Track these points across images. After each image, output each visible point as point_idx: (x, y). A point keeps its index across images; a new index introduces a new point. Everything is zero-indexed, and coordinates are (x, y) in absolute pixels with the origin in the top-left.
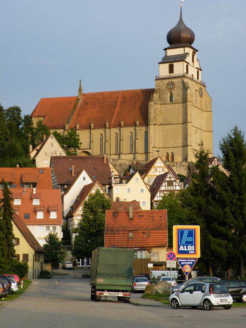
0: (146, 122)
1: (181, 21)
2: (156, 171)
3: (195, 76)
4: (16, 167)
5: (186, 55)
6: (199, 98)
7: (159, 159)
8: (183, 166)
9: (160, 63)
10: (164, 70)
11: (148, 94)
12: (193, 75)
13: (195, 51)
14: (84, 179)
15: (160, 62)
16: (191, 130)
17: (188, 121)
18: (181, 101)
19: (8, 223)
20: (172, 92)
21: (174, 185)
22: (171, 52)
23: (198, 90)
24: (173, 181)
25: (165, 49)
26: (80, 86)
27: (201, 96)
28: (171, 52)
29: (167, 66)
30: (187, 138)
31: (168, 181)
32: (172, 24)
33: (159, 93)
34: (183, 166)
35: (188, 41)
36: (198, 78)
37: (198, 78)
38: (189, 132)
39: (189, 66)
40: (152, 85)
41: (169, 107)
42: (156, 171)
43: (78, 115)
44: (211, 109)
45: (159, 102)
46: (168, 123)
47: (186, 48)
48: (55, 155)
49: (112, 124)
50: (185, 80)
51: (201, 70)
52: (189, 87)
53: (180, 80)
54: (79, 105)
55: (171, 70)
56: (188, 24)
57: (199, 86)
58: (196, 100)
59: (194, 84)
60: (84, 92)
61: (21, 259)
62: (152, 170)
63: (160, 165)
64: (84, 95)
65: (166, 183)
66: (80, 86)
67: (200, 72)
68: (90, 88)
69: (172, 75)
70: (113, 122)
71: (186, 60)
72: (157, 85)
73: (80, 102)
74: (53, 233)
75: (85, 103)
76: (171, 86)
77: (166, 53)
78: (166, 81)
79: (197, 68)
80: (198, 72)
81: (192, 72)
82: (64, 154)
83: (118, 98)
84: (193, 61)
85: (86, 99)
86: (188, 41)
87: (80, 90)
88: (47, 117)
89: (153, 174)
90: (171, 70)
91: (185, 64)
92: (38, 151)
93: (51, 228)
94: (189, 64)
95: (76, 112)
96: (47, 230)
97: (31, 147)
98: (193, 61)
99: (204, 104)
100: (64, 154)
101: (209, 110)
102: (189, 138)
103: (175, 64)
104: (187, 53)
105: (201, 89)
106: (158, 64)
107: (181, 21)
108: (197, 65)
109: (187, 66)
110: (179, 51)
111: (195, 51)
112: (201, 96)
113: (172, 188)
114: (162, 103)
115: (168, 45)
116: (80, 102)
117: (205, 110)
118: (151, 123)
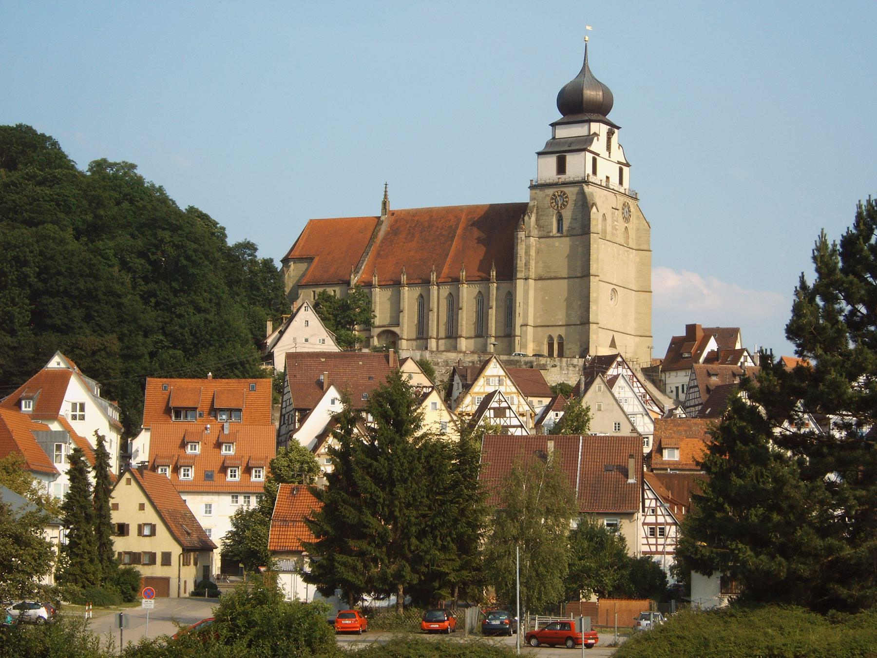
0: (508, 272)
1: (585, 69)
2: (488, 384)
4: (206, 377)
5: (589, 139)
6: (621, 225)
7: (495, 360)
8: (574, 366)
9: (539, 154)
10: (548, 169)
11: (517, 212)
12: (607, 178)
13: (613, 127)
14: (333, 402)
15: (541, 148)
16: (599, 291)
17: (591, 272)
18: (579, 232)
19: (101, 507)
20: (563, 212)
21: (508, 415)
22: (564, 132)
23: (620, 207)
24: (505, 408)
25: (553, 125)
26: (386, 195)
27: (627, 219)
28: (564, 132)
29: (552, 161)
30: (589, 308)
31: (494, 409)
32: (567, 77)
33: (537, 213)
34: (574, 366)
35: (600, 110)
36: (621, 182)
37: (621, 182)
38: (593, 295)
40: (521, 195)
41: (557, 243)
42: (488, 384)
43: (378, 255)
44: (649, 244)
45: (536, 232)
46: (552, 275)
47: (592, 124)
48: (293, 350)
49: (442, 275)
50: (588, 189)
51: (627, 165)
52: (594, 204)
54: (381, 234)
55: (561, 168)
56: (598, 72)
57: (622, 199)
58: (614, 228)
59: (610, 195)
60: (393, 206)
61: (116, 556)
62: (481, 381)
64: (393, 214)
65: (492, 411)
66: (386, 195)
67: (626, 170)
68: (407, 199)
69: (563, 178)
70: (446, 270)
71: (592, 148)
72: (532, 199)
73: (384, 229)
74: (245, 508)
75: (394, 231)
76: (559, 202)
77: (554, 132)
78: (550, 192)
79: (619, 163)
80: (621, 170)
81: (607, 169)
82: (331, 346)
83: (458, 221)
84: (609, 148)
85: (396, 221)
86: (600, 110)
87: (385, 204)
88: (316, 260)
89: (482, 391)
90: (561, 168)
91: (589, 157)
92: (282, 333)
93: (241, 499)
94: (598, 155)
95: (373, 250)
96: (233, 502)
97: (269, 325)
98: (609, 148)
99: (632, 234)
100: (331, 346)
101: (645, 247)
102: (593, 308)
103: (570, 159)
104: (595, 134)
106: (536, 155)
107: (585, 69)
108: (618, 155)
109: (594, 161)
110: (577, 131)
111: (613, 127)
112: (627, 219)
114: (545, 233)
115: (558, 116)
116: (384, 229)
117: (637, 248)
118: (519, 275)
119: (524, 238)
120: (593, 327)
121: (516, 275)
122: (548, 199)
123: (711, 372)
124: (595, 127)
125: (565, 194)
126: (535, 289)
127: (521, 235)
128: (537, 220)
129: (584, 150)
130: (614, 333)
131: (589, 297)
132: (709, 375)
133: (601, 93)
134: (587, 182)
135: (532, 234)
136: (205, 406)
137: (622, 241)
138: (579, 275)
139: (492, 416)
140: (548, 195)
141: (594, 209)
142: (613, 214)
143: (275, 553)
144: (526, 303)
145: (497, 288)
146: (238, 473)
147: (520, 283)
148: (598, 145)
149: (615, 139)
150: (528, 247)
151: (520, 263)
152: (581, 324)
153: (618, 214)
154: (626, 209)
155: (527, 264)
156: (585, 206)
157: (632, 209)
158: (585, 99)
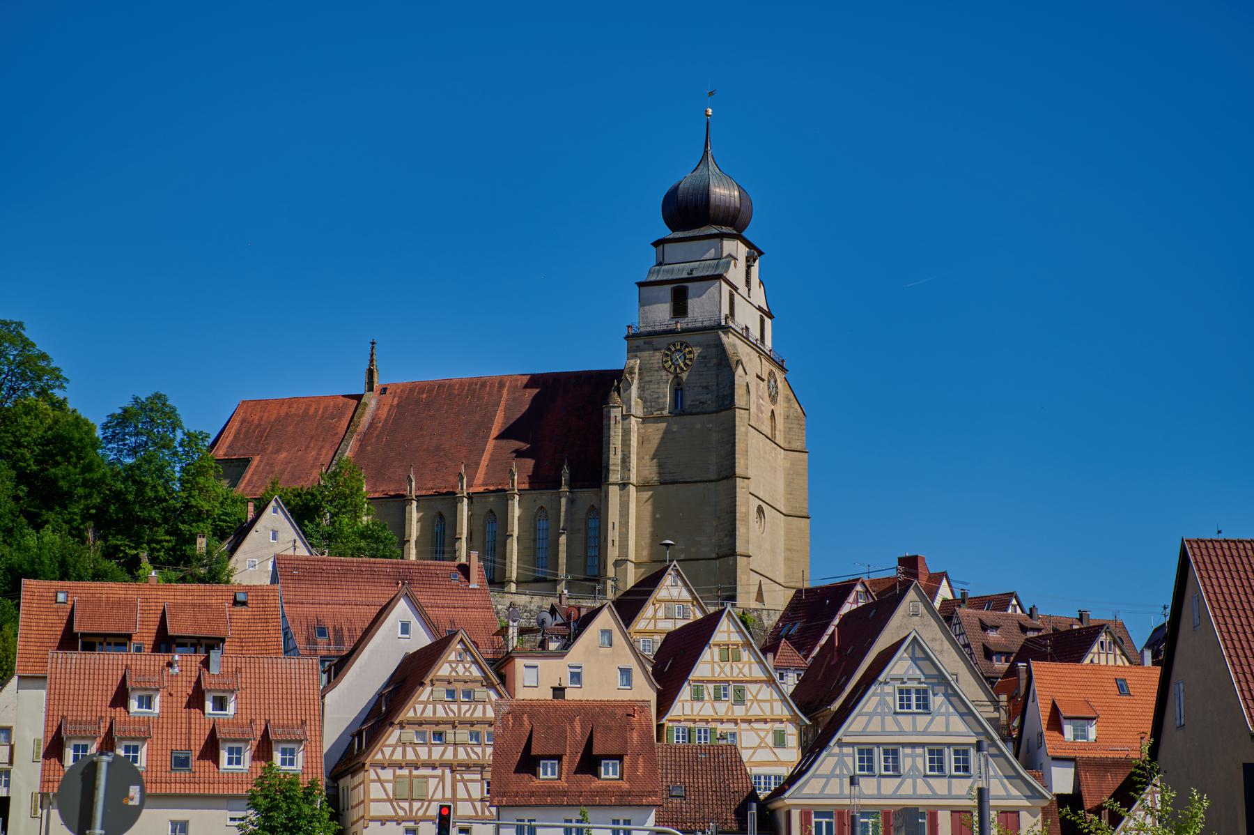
3: (755, 333)
6: (767, 406)
27: (773, 399)
33: (640, 379)
39: (737, 297)
50: (729, 340)
51: (771, 317)
52: (739, 362)
55: (680, 309)
58: (759, 407)
63: (675, 593)
65: (716, 650)
67: (768, 322)
79: (760, 309)
84: (748, 283)
90: (680, 309)
94: (736, 289)
98: (748, 283)
105: (771, 374)
112: (773, 399)
113: (736, 671)
118: (615, 477)
119: (619, 418)
120: (741, 561)
121: (607, 477)
123: (988, 623)
124: (730, 246)
126: (638, 501)
127: (616, 413)
128: (641, 388)
129: (719, 277)
130: (764, 580)
131: (734, 512)
132: (984, 627)
133: (736, 193)
134: (726, 329)
135: (633, 411)
136: (145, 634)
137: (768, 432)
138: (713, 478)
139: (717, 658)
141: (740, 371)
142: (758, 385)
143: (779, 792)
144: (624, 524)
145: (571, 502)
146: (247, 756)
147: (614, 492)
148: (736, 274)
149: (755, 270)
150: (626, 433)
151: (615, 459)
152: (718, 557)
153: (764, 385)
154: (772, 382)
155: (625, 460)
156: (724, 366)
157: (780, 385)
158: (712, 197)
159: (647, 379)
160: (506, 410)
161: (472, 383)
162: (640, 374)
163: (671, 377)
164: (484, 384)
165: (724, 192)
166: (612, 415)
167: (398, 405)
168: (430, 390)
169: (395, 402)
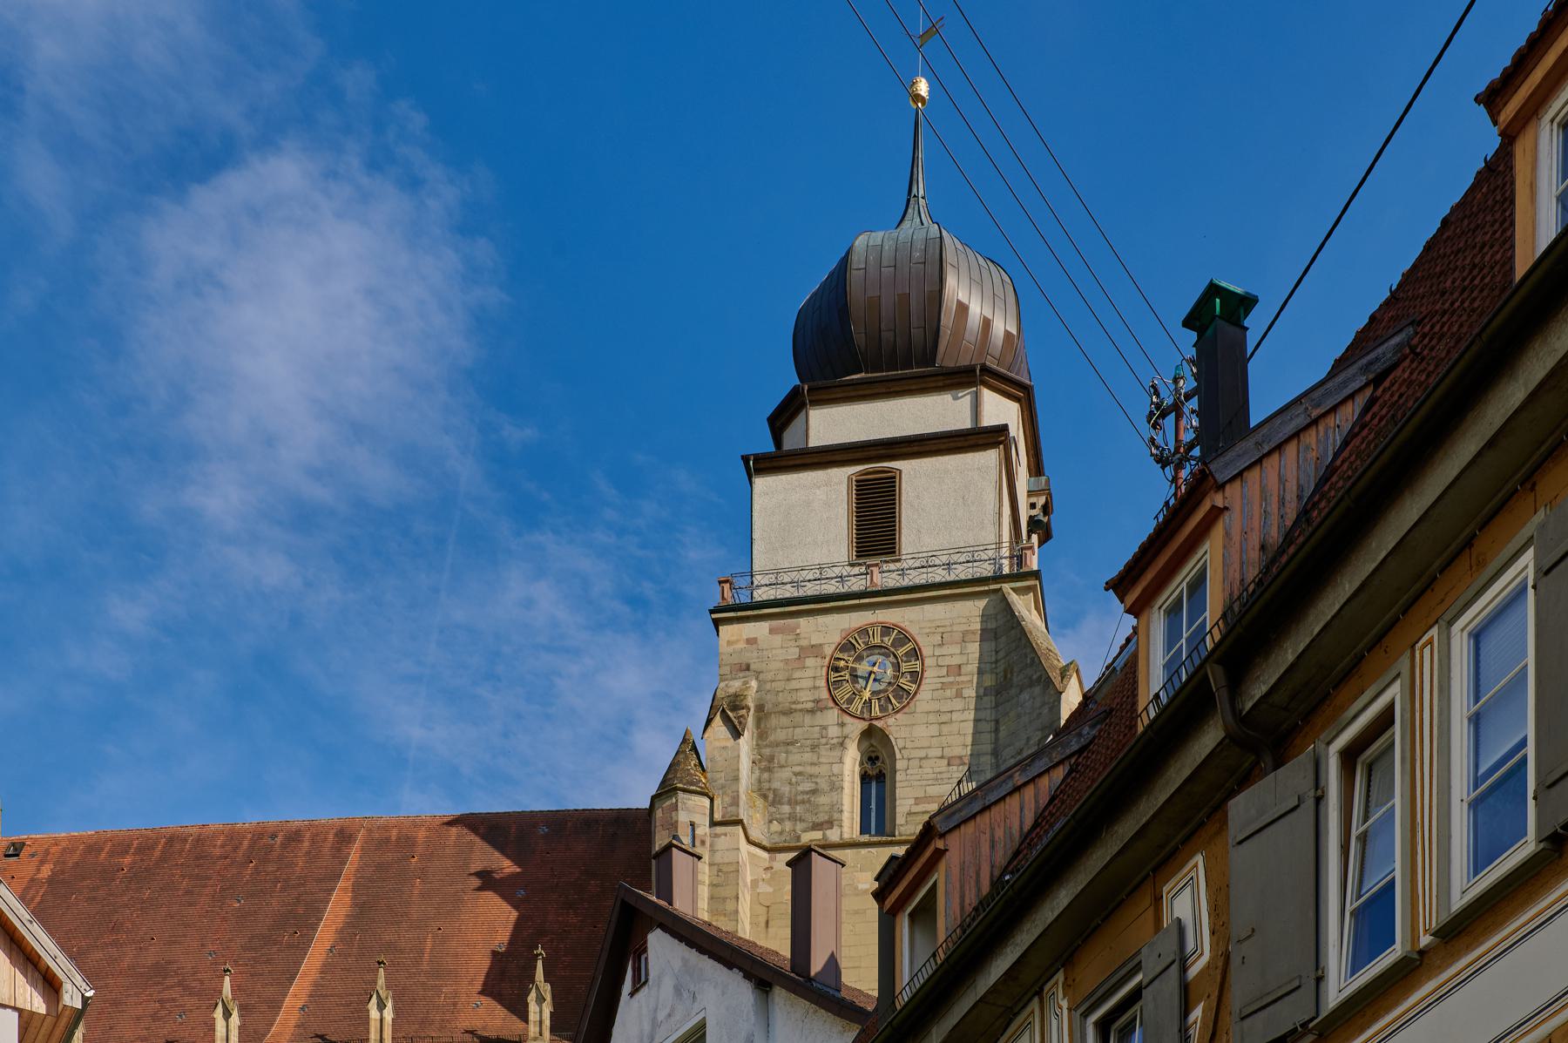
20: (895, 726)
33: (762, 735)
53: (970, 612)
55: (876, 525)
69: (886, 576)
78: (829, 629)
90: (876, 525)
103: (913, 473)
119: (703, 830)
122: (815, 669)
125: (904, 638)
128: (766, 764)
140: (815, 650)
159: (781, 735)
160: (356, 889)
161: (261, 834)
162: (758, 721)
163: (856, 727)
164: (294, 837)
165: (977, 303)
166: (683, 817)
167: (51, 881)
168: (140, 850)
169: (46, 871)
